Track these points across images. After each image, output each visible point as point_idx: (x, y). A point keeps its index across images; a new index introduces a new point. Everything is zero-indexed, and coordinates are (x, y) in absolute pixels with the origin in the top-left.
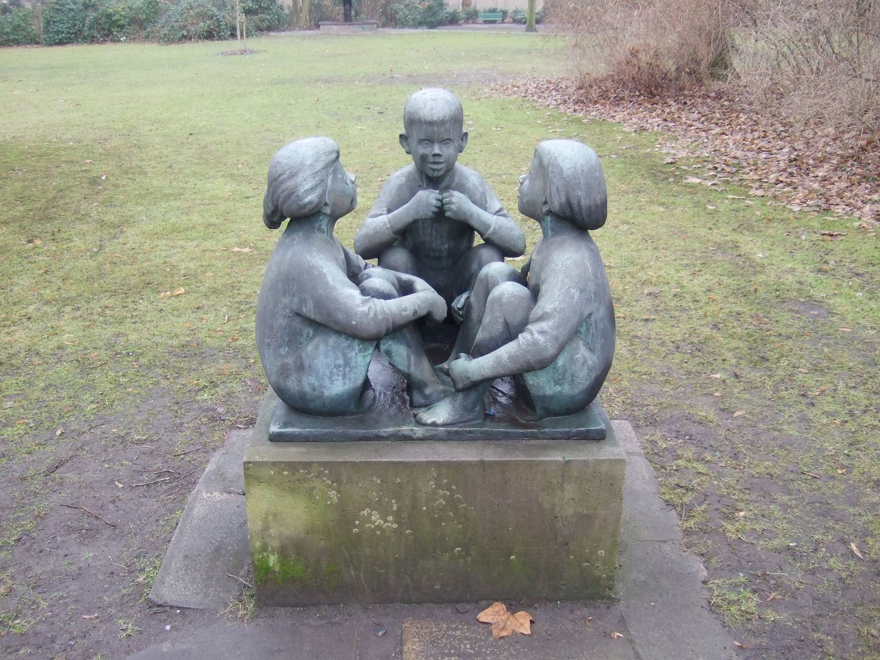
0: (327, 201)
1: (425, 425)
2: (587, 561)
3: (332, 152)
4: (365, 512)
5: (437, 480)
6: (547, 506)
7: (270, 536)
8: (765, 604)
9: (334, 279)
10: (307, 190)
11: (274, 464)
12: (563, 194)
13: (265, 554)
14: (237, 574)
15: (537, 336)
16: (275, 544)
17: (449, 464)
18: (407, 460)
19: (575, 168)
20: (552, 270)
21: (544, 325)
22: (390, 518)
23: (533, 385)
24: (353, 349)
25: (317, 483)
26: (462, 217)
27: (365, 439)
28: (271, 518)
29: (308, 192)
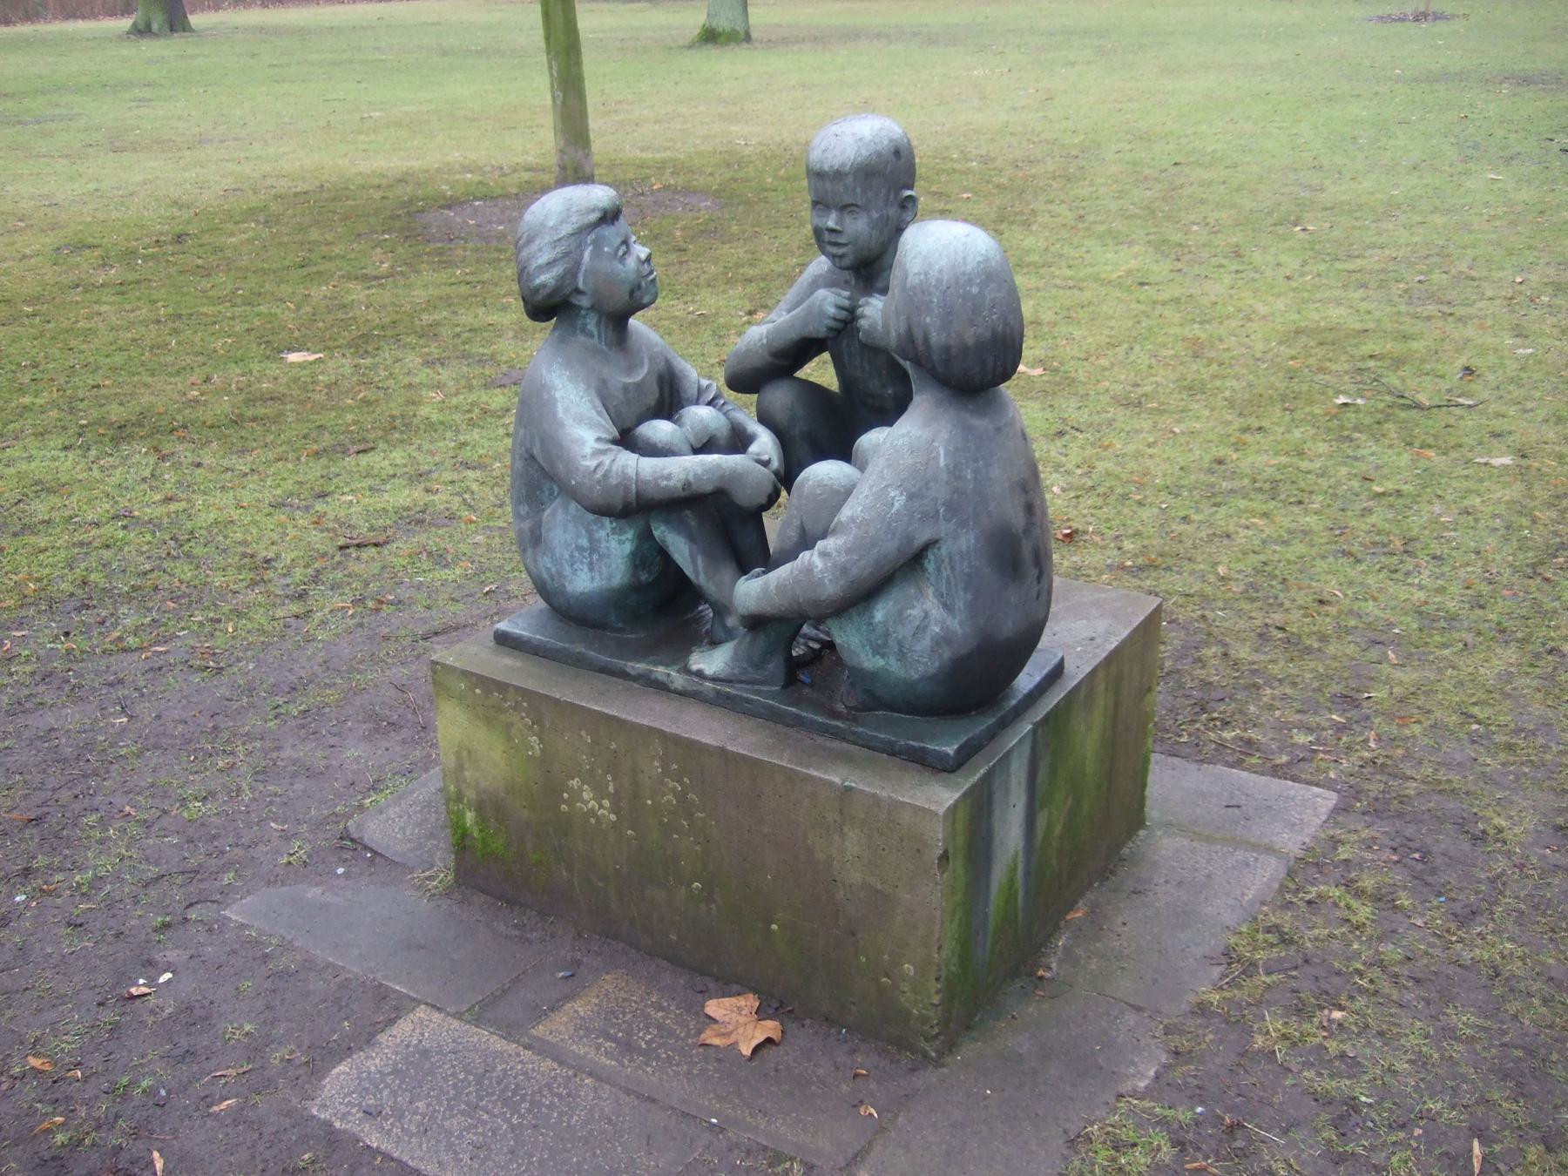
0: (581, 286)
3: (593, 210)
4: (575, 783)
6: (820, 856)
9: (567, 410)
11: (465, 674)
16: (470, 794)
19: (926, 273)
25: (513, 717)
27: (605, 670)
28: (465, 754)
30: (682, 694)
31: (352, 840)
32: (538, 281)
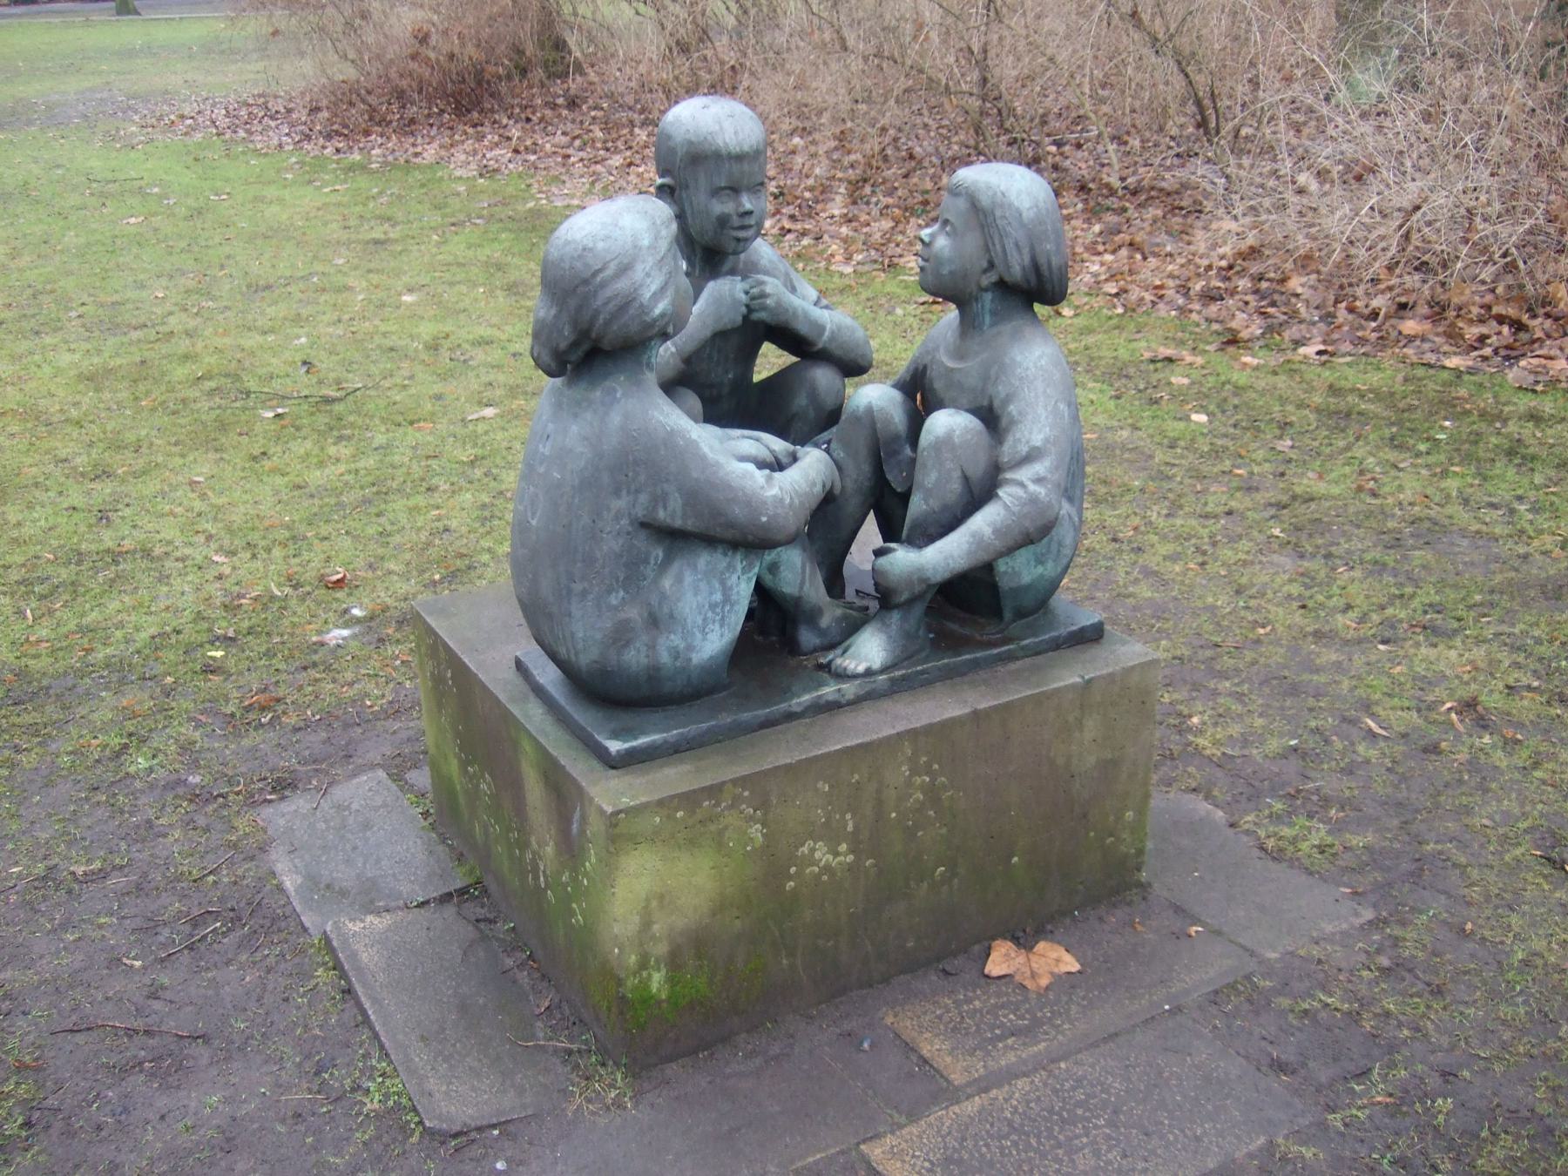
1: (855, 676)
2: (1111, 835)
5: (912, 761)
6: (1060, 761)
7: (653, 938)
8: (1337, 828)
9: (711, 448)
10: (655, 294)
11: (661, 803)
12: (1026, 251)
13: (645, 974)
14: (533, 1037)
15: (1032, 487)
16: (661, 949)
17: (929, 730)
18: (867, 739)
20: (1021, 379)
21: (1039, 468)
22: (843, 847)
23: (1005, 573)
24: (735, 569)
25: (731, 819)
26: (782, 318)
28: (654, 904)
29: (656, 296)
30: (858, 701)
31: (456, 1135)
32: (657, 311)
